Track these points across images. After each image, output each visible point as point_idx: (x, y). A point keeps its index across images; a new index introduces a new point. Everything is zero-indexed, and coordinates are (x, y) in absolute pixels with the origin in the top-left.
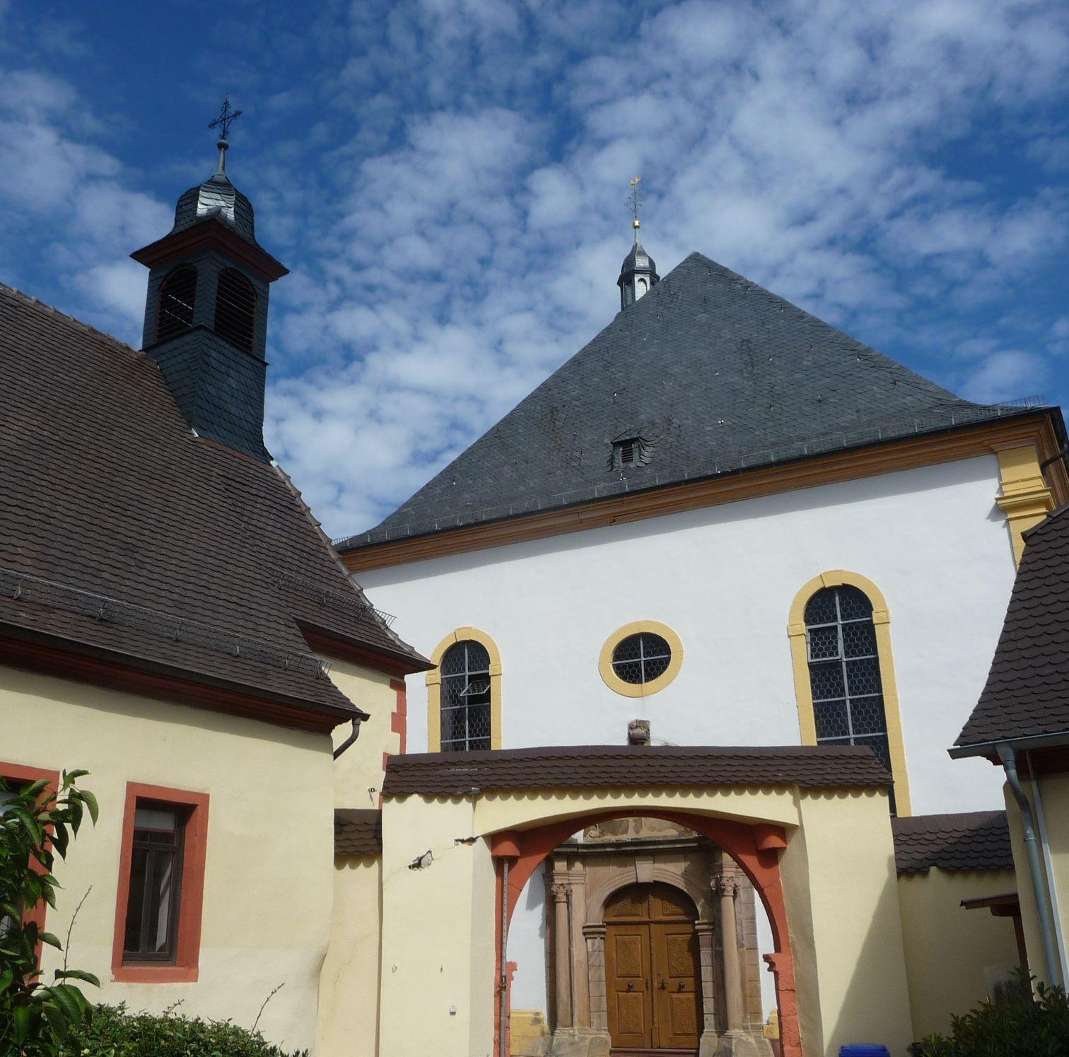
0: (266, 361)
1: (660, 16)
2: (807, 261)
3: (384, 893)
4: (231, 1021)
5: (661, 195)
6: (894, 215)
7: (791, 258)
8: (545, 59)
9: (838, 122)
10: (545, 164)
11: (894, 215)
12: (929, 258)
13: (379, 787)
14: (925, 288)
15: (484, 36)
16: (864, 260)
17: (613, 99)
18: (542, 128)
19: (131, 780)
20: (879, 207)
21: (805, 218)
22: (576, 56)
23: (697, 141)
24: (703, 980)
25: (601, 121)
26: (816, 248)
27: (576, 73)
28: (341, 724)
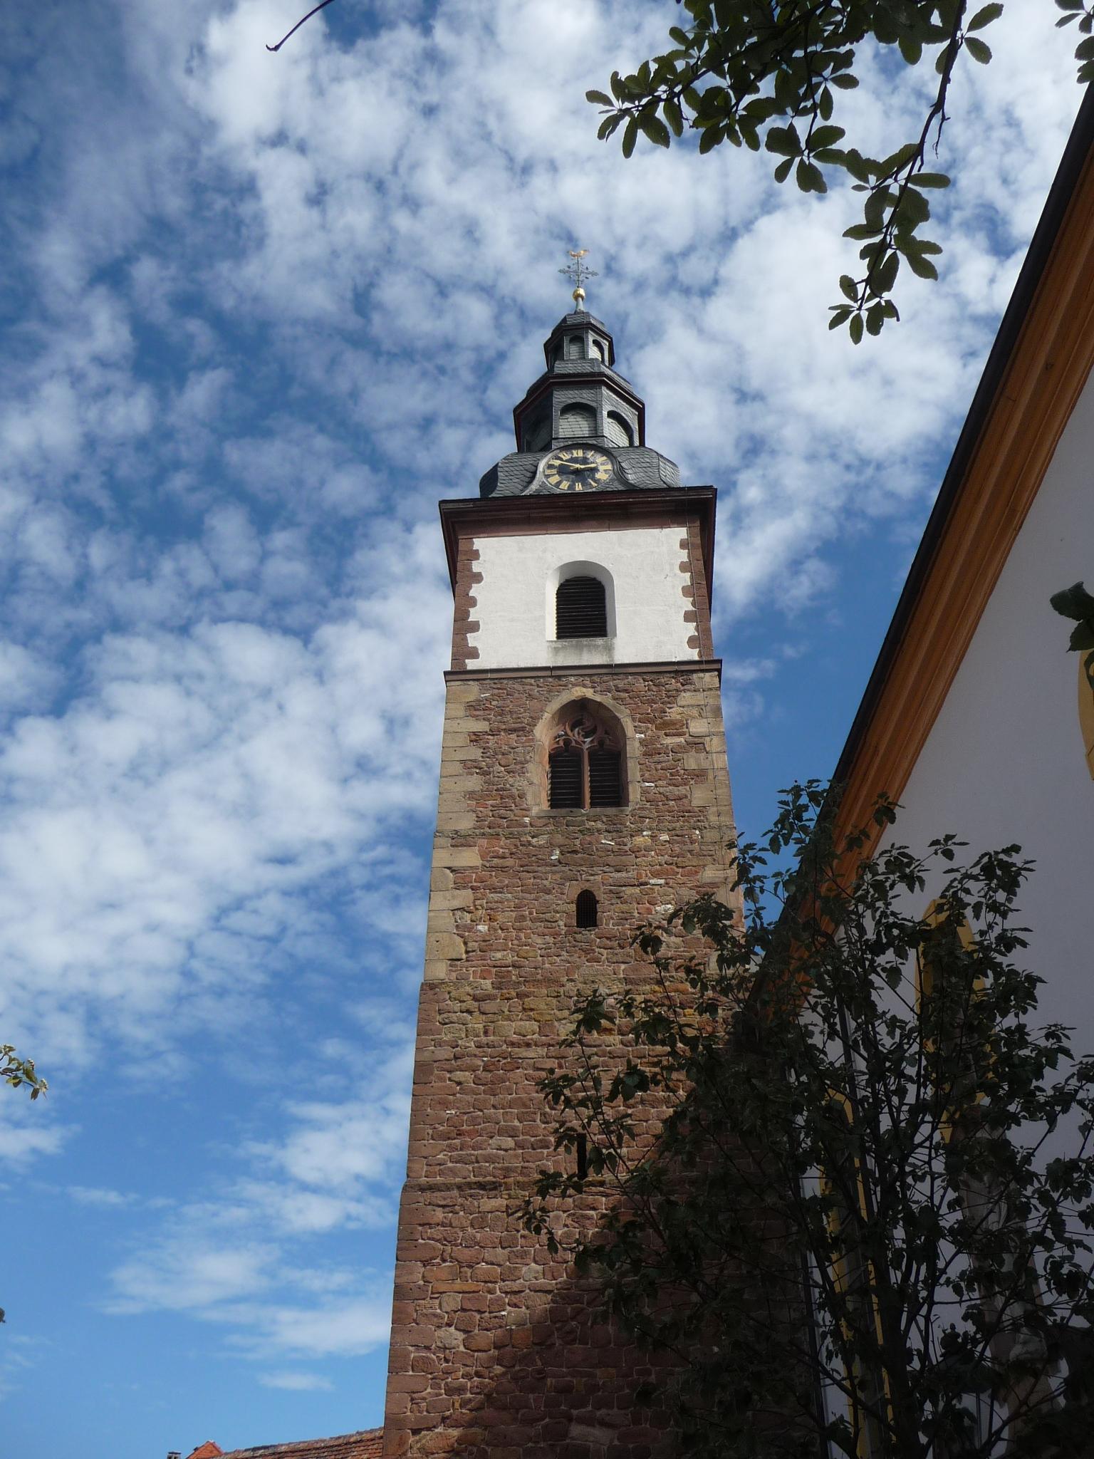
0: (685, 477)
1: (220, 626)
2: (273, 904)
3: (517, 403)
4: (995, 24)
5: (148, 783)
6: (369, 887)
7: (259, 895)
8: (84, 615)
9: (345, 781)
10: (43, 714)
11: (369, 887)
12: (387, 935)
13: (929, 281)
14: (374, 960)
15: (31, 571)
16: (327, 918)
17: (136, 679)
18: (50, 676)
19: (663, 148)
20: (358, 876)
21: (283, 860)
22: (119, 625)
23: (206, 744)
24: (920, 1130)
25: (118, 693)
26: (286, 893)
27: (114, 642)
28: (874, 161)
